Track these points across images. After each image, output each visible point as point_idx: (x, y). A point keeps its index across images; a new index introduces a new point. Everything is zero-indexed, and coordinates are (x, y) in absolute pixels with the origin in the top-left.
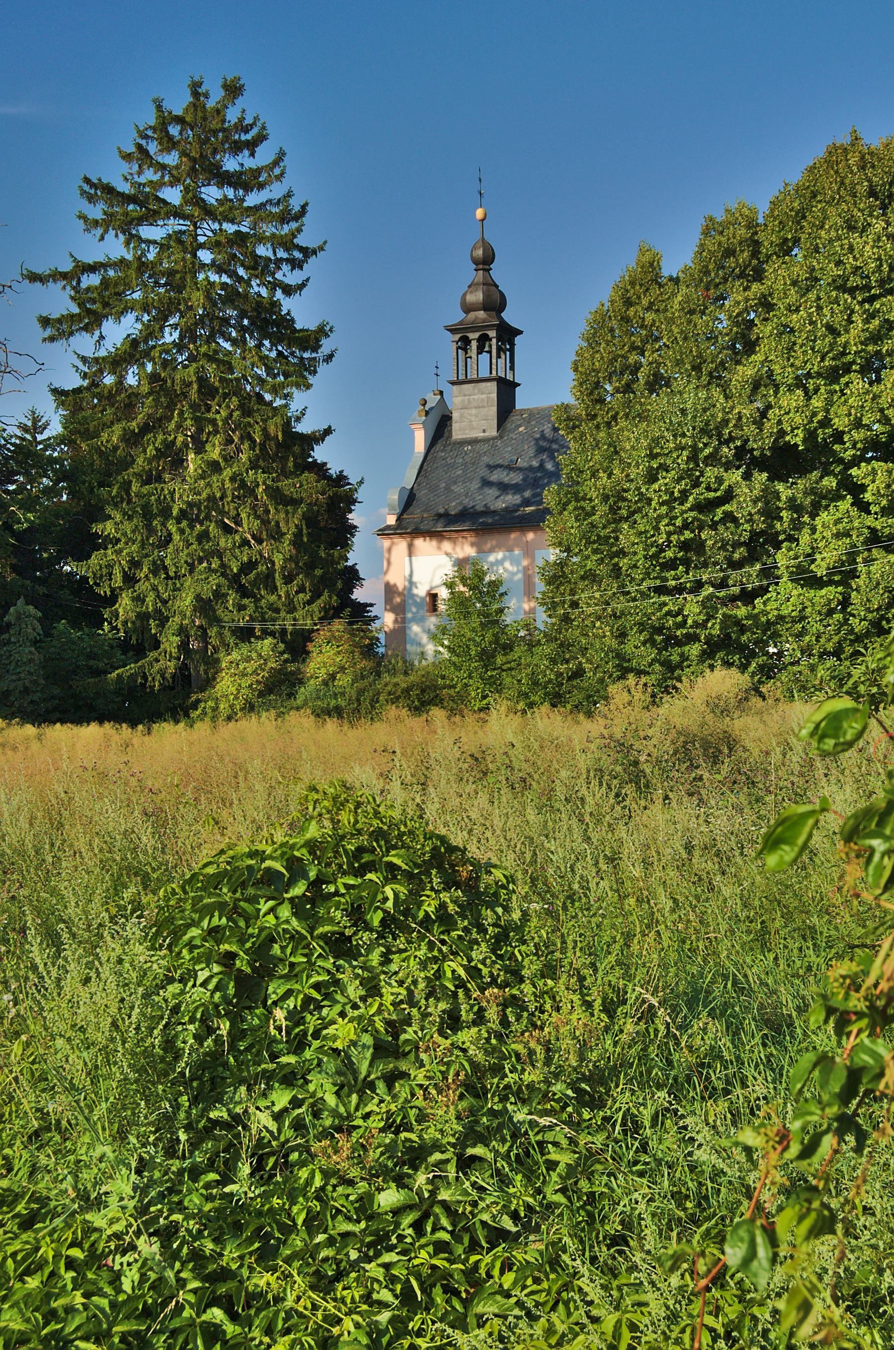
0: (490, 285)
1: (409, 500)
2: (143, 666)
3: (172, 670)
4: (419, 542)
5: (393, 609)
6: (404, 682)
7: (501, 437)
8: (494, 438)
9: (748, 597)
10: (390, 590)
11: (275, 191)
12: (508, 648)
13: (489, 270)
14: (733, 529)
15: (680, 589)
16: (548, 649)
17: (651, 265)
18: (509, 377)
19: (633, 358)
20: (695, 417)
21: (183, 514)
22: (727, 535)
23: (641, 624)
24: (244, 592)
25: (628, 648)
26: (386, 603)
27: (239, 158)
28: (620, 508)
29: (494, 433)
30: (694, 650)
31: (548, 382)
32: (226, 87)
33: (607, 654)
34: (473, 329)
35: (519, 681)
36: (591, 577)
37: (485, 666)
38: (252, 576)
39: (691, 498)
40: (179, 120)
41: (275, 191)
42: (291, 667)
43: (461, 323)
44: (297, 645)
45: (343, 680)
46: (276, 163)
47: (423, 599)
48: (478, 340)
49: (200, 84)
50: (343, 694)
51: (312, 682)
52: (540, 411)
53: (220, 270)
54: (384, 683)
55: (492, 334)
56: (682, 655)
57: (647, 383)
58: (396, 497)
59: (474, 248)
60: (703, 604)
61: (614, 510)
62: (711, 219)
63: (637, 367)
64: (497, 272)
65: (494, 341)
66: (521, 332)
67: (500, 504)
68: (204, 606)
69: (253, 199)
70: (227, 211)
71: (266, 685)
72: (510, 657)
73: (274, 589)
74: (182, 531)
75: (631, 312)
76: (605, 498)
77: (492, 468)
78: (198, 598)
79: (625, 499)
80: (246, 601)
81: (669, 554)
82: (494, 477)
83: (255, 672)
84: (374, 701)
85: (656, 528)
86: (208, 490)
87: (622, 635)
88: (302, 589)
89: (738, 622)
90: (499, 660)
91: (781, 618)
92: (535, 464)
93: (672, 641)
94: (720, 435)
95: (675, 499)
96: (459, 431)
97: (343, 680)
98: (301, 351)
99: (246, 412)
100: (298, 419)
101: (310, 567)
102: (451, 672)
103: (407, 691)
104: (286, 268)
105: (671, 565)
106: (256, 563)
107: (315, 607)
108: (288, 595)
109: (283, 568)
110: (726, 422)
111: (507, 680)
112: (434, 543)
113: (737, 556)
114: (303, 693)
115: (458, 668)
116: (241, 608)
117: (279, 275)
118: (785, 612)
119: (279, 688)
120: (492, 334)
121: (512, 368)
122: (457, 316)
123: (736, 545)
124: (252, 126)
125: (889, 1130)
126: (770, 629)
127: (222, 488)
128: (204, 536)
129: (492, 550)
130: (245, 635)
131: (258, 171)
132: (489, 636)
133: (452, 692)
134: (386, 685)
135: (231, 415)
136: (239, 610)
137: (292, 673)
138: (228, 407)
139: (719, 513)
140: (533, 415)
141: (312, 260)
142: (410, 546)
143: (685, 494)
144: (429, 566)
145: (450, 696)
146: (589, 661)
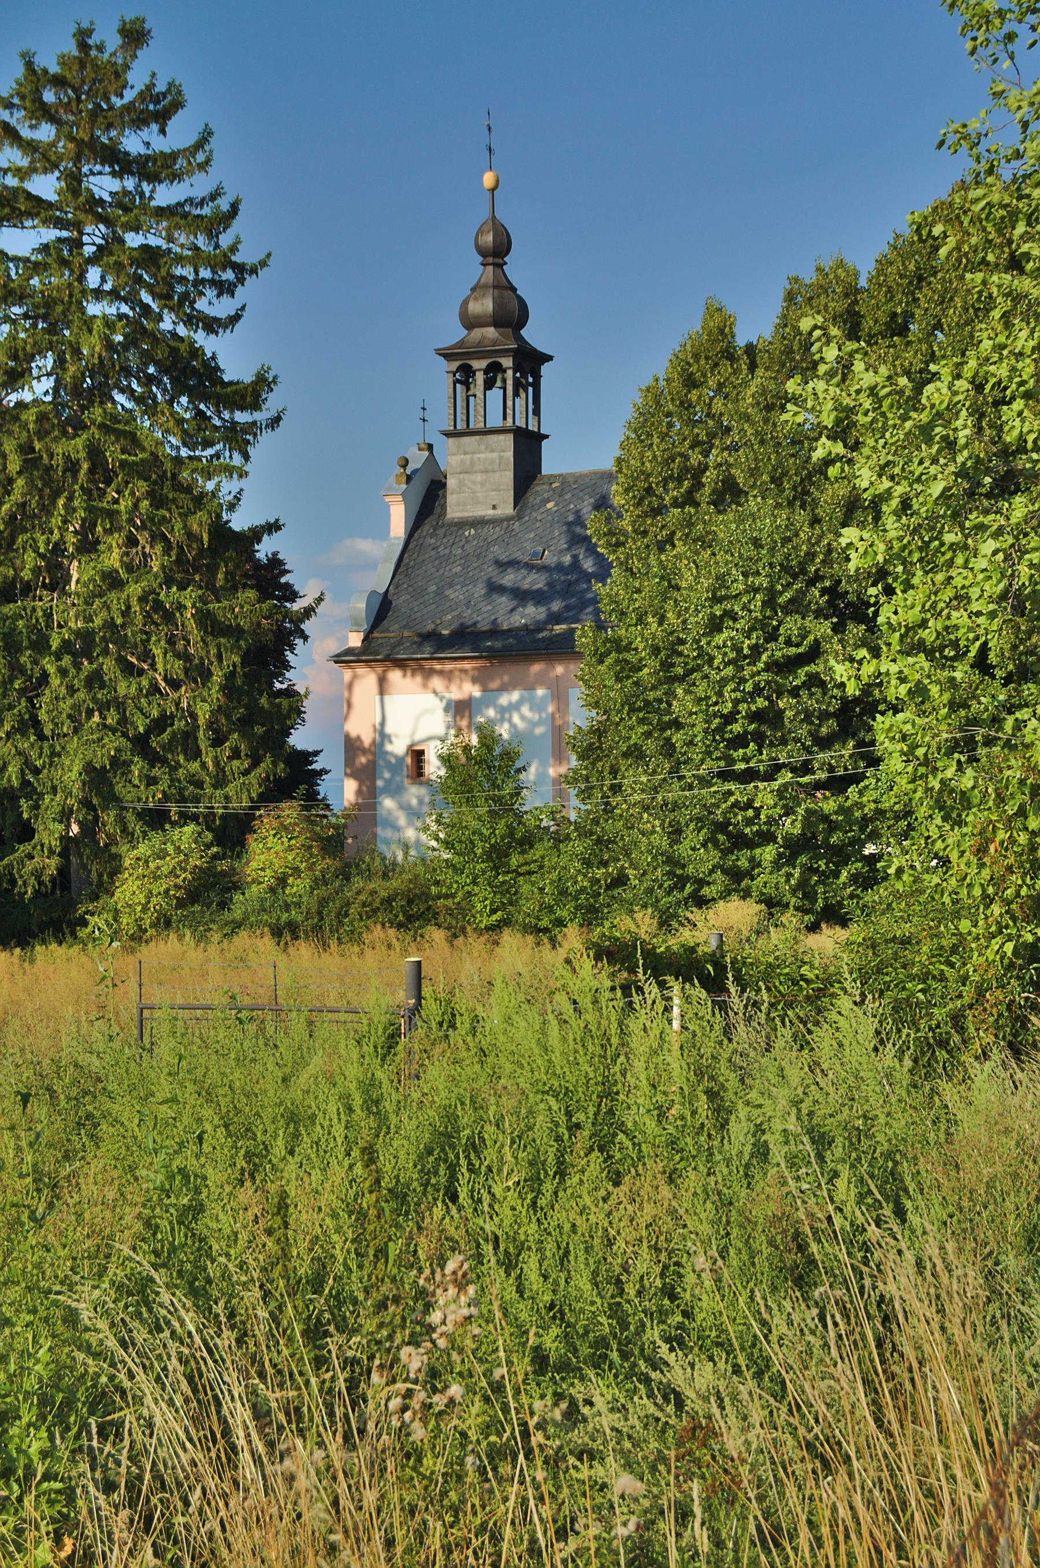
0: (504, 287)
1: (382, 610)
2: (10, 865)
3: (52, 871)
4: (395, 676)
5: (355, 774)
6: (383, 888)
7: (519, 517)
8: (509, 519)
9: (837, 784)
10: (352, 746)
11: (197, 186)
12: (527, 842)
13: (500, 266)
14: (819, 695)
15: (749, 776)
16: (579, 846)
17: (722, 331)
18: (532, 427)
19: (695, 458)
20: (772, 549)
21: (66, 646)
22: (812, 704)
23: (699, 820)
24: (153, 759)
25: (683, 850)
26: (346, 765)
27: (145, 134)
28: (673, 665)
29: (508, 510)
30: (768, 853)
31: (588, 435)
32: (124, 32)
33: (655, 858)
34: (479, 355)
35: (541, 890)
36: (636, 754)
37: (495, 868)
38: (165, 736)
39: (764, 657)
40: (59, 82)
41: (197, 186)
42: (223, 866)
43: (461, 344)
44: (232, 833)
45: (298, 886)
46: (199, 145)
47: (400, 760)
48: (486, 371)
49: (89, 33)
50: (298, 905)
51: (254, 888)
52: (578, 478)
53: (115, 295)
54: (353, 890)
55: (507, 362)
56: (752, 860)
57: (714, 491)
58: (363, 606)
59: (480, 231)
60: (780, 793)
61: (667, 666)
62: (796, 280)
63: (703, 469)
64: (515, 268)
65: (510, 373)
66: (550, 358)
67: (518, 620)
68: (98, 778)
69: (165, 195)
70: (129, 210)
71: (189, 892)
72: (529, 857)
73: (197, 754)
74: (63, 672)
75: (694, 395)
76: (656, 650)
77: (503, 565)
78: (89, 768)
79: (680, 654)
80: (156, 772)
81: (737, 728)
82: (509, 579)
83: (172, 872)
84: (342, 914)
85: (720, 694)
86: (104, 614)
87: (676, 833)
88: (236, 754)
89: (825, 818)
90: (514, 861)
91: (880, 813)
92: (567, 559)
93: (740, 842)
94: (803, 571)
95: (745, 657)
96: (458, 504)
97: (298, 886)
98: (228, 408)
99: (158, 501)
100: (232, 507)
101: (244, 724)
102: (446, 876)
103: (388, 901)
104: (210, 293)
105: (740, 741)
106: (172, 716)
107: (253, 778)
108: (216, 762)
109: (210, 725)
110: (811, 556)
111: (525, 888)
112: (419, 679)
113: (824, 730)
114: (240, 904)
115: (458, 870)
116: (152, 781)
117: (201, 305)
118: (885, 805)
119: (207, 896)
120: (507, 362)
121: (537, 412)
122: (455, 334)
123: (824, 716)
124: (164, 95)
125: (9, 446)
126: (869, 825)
127: (126, 613)
128: (95, 680)
129: (504, 688)
130: (156, 819)
131: (174, 156)
132: (501, 827)
133: (449, 903)
134: (359, 893)
135: (136, 505)
136: (148, 785)
137: (223, 874)
138: (132, 494)
139: (802, 673)
140: (567, 484)
141: (250, 280)
142: (382, 681)
143: (756, 651)
144: (413, 713)
145: (448, 909)
146: (634, 866)
